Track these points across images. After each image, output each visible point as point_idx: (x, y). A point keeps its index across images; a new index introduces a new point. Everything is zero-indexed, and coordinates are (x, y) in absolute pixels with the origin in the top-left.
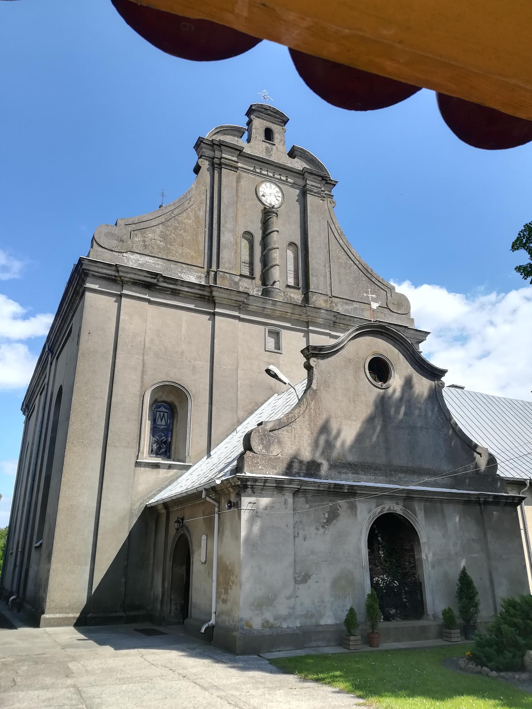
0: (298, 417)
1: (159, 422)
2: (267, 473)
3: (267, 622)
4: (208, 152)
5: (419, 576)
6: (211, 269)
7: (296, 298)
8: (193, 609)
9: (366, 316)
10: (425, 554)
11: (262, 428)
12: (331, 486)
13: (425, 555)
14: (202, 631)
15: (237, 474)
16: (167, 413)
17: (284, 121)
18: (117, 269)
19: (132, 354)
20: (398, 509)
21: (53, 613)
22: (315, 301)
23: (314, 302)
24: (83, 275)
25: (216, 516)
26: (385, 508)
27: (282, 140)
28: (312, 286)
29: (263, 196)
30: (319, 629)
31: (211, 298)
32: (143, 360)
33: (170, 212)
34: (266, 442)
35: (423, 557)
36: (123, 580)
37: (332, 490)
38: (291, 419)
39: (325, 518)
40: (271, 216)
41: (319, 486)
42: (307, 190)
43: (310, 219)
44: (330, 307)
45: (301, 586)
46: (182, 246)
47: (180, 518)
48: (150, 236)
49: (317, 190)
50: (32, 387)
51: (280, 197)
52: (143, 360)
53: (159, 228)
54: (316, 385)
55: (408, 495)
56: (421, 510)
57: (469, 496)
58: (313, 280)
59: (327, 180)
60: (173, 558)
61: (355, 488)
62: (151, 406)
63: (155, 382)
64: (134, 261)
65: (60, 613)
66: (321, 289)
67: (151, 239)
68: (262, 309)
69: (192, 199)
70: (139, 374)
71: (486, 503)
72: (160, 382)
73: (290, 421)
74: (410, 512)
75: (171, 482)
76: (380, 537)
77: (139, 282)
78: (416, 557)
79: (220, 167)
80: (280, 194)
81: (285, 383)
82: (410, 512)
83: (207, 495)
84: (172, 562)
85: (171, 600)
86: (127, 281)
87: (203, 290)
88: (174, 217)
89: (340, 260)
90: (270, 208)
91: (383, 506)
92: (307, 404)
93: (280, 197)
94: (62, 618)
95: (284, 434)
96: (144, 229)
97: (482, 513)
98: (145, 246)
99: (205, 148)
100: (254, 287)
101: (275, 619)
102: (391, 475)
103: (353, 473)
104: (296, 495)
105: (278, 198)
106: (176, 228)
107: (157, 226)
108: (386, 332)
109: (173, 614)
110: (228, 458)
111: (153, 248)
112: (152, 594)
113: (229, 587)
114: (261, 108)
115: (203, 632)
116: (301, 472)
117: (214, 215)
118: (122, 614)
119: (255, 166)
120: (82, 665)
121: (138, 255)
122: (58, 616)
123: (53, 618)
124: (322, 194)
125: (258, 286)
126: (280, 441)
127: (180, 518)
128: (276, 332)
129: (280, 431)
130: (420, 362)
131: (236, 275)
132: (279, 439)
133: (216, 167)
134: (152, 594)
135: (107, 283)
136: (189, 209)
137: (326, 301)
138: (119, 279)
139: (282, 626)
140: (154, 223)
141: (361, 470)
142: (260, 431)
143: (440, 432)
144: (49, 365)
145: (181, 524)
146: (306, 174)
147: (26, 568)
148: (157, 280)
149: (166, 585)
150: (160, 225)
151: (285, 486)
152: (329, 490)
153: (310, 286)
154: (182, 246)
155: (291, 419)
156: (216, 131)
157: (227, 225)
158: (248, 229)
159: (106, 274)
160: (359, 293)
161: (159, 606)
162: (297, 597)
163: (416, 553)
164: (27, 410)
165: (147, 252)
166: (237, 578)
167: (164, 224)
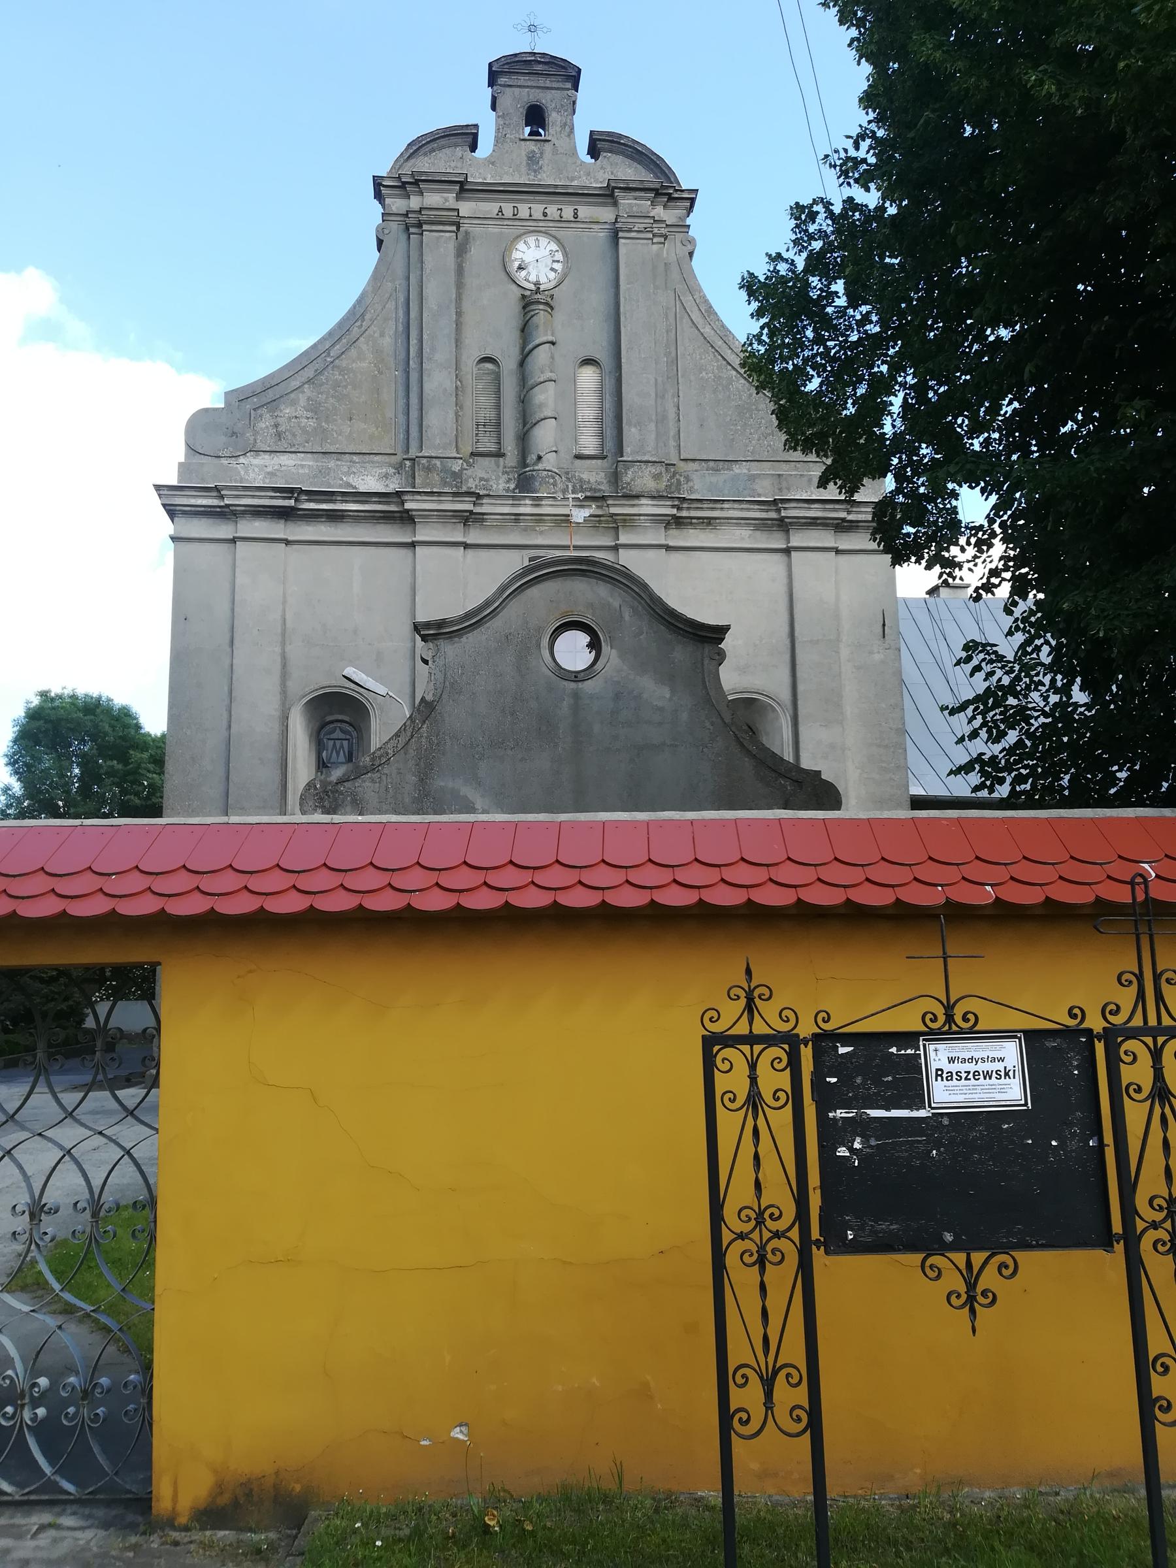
7: (592, 480)
9: (760, 491)
16: (347, 741)
17: (569, 75)
22: (632, 480)
23: (629, 484)
27: (565, 124)
28: (629, 449)
29: (520, 268)
33: (324, 355)
38: (380, 759)
40: (532, 313)
43: (625, 298)
48: (288, 411)
51: (558, 261)
58: (631, 434)
63: (307, 690)
66: (649, 452)
67: (290, 418)
69: (368, 317)
70: (276, 678)
72: (317, 690)
73: (378, 762)
77: (262, 509)
80: (559, 256)
87: (387, 503)
88: (332, 362)
89: (704, 373)
92: (413, 729)
93: (558, 261)
96: (275, 400)
98: (279, 435)
99: (390, 196)
100: (500, 474)
106: (337, 384)
107: (300, 390)
108: (592, 569)
111: (294, 435)
121: (267, 456)
125: (508, 470)
136: (362, 339)
137: (657, 477)
142: (318, 786)
146: (617, 193)
150: (306, 386)
154: (351, 419)
155: (380, 759)
156: (412, 151)
158: (488, 353)
165: (283, 446)
167: (313, 383)
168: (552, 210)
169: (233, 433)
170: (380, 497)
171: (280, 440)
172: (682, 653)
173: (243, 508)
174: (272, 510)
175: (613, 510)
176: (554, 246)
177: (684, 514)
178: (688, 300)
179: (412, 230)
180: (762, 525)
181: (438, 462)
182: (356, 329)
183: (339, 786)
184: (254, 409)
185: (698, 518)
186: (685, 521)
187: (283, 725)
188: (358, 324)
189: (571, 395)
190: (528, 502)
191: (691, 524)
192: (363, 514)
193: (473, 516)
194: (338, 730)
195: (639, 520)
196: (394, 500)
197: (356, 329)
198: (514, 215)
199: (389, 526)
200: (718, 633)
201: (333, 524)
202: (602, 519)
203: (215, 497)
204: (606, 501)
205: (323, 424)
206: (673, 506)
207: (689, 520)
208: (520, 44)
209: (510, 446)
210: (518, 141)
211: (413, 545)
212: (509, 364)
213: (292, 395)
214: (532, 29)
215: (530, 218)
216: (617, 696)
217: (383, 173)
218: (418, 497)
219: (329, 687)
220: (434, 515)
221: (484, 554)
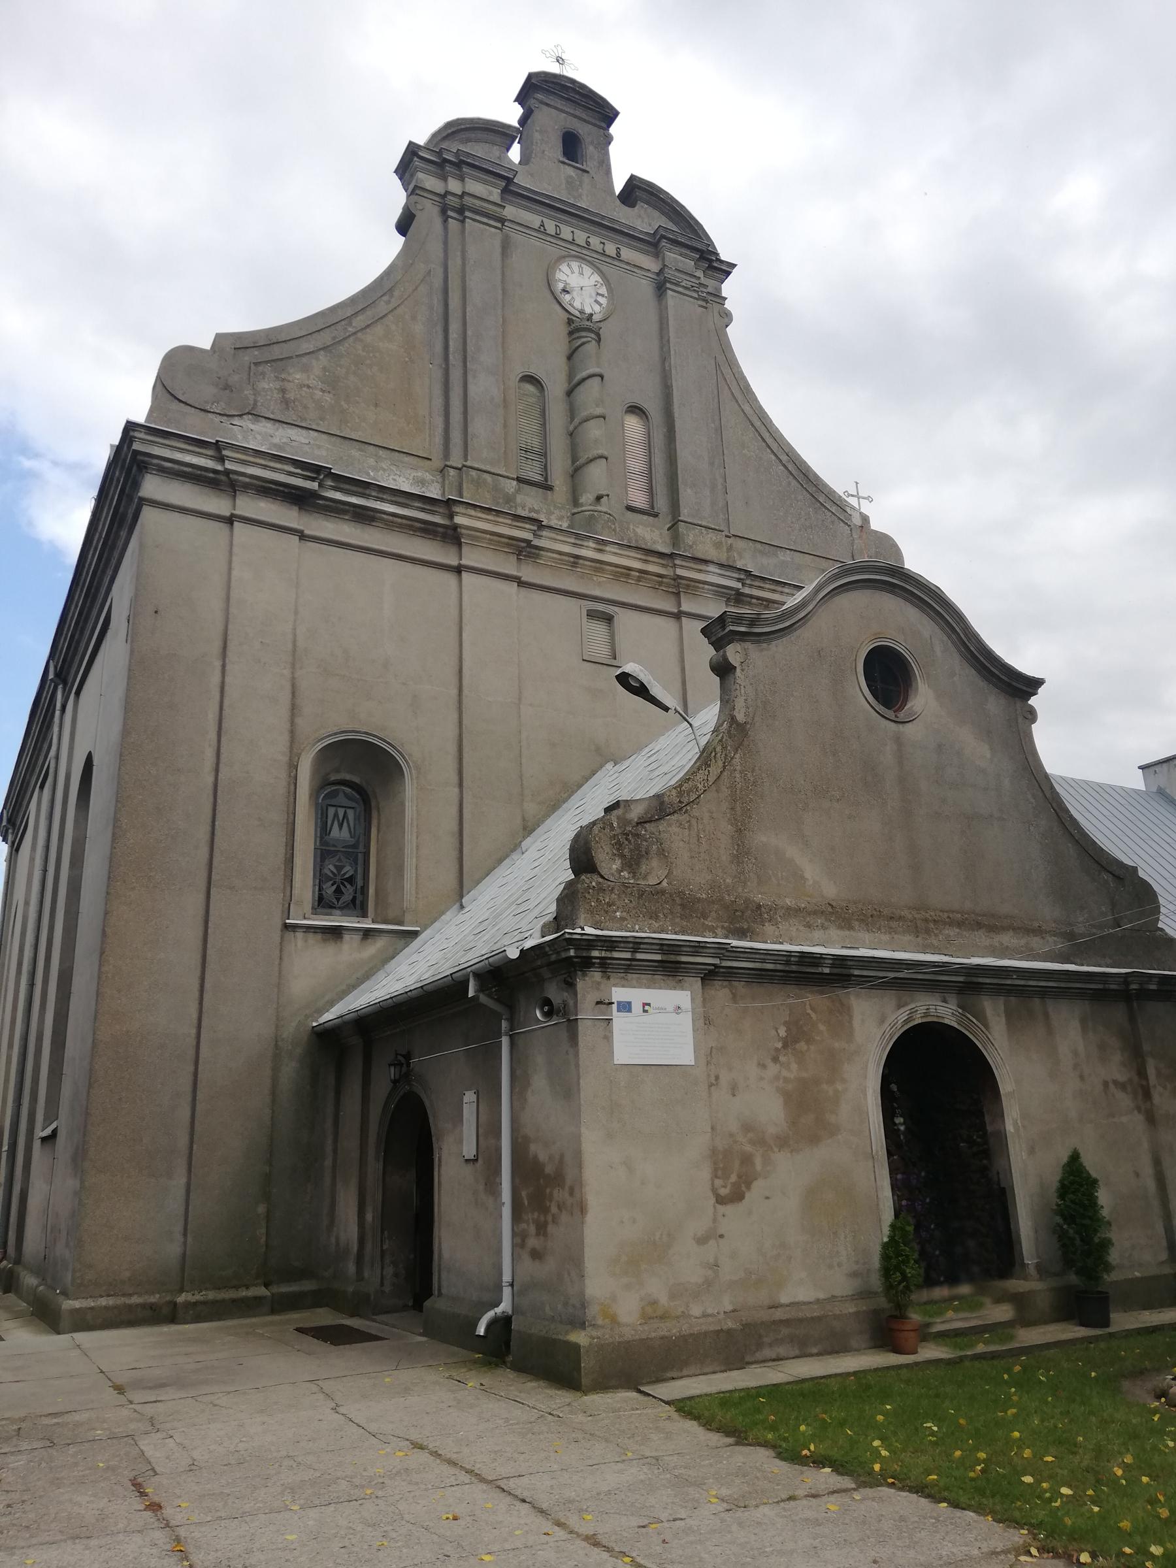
0: (705, 791)
1: (335, 833)
2: (637, 927)
3: (654, 1303)
4: (431, 182)
5: (998, 1173)
6: (448, 463)
8: (444, 1276)
10: (1013, 1120)
11: (618, 818)
12: (792, 959)
13: (1011, 1122)
14: (480, 1331)
15: (567, 931)
19: (265, 663)
20: (946, 1011)
21: (91, 1297)
23: (691, 547)
24: (135, 468)
25: (505, 1041)
26: (917, 1011)
29: (565, 291)
30: (779, 1315)
31: (450, 532)
32: (293, 678)
33: (343, 323)
34: (631, 850)
35: (1007, 1129)
36: (261, 1209)
37: (794, 968)
39: (780, 1039)
41: (763, 961)
42: (666, 280)
44: (728, 559)
45: (728, 1209)
46: (376, 405)
47: (401, 1055)
49: (691, 283)
50: (21, 773)
51: (603, 296)
52: (293, 678)
53: (317, 359)
54: (743, 710)
56: (999, 1015)
57: (1104, 979)
58: (687, 495)
59: (711, 261)
60: (385, 1152)
61: (849, 963)
62: (315, 793)
63: (323, 732)
64: (259, 437)
65: (108, 1296)
67: (301, 386)
69: (396, 293)
70: (284, 711)
71: (1144, 995)
73: (685, 800)
74: (974, 1020)
75: (367, 974)
76: (894, 1083)
77: (274, 487)
78: (989, 1128)
79: (461, 218)
80: (603, 290)
81: (666, 709)
82: (974, 1020)
83: (481, 988)
84: (381, 1163)
85: (383, 1252)
88: (355, 333)
91: (913, 1006)
93: (603, 296)
94: (116, 1307)
95: (672, 831)
97: (1132, 1019)
98: (286, 403)
101: (672, 1297)
102: (928, 931)
103: (840, 928)
104: (707, 982)
105: (600, 299)
109: (387, 1288)
110: (519, 901)
112: (333, 1240)
113: (550, 1218)
114: (553, 83)
115: (482, 1334)
116: (717, 926)
117: (450, 331)
118: (262, 1291)
119: (544, 219)
120: (179, 1444)
121: (269, 425)
122: (103, 1302)
123: (92, 1308)
124: (700, 293)
126: (663, 850)
127: (401, 1055)
128: (605, 617)
129: (662, 825)
130: (982, 659)
131: (508, 477)
132: (661, 844)
133: (452, 218)
134: (333, 1240)
135: (196, 488)
137: (718, 545)
138: (223, 478)
139: (691, 1313)
140: (306, 346)
141: (857, 920)
142: (615, 824)
143: (1032, 828)
144: (57, 713)
145: (404, 1069)
146: (664, 243)
147: (22, 1190)
149: (369, 1217)
151: (684, 959)
152: (787, 969)
153: (681, 509)
158: (533, 370)
160: (790, 529)
161: (351, 1268)
162: (721, 1236)
163: (987, 1119)
164: (10, 831)
165: (291, 417)
166: (571, 1193)
168: (595, 241)
169: (227, 385)
170: (424, 503)
171: (288, 408)
172: (995, 704)
173: (247, 480)
174: (286, 490)
175: (679, 572)
176: (596, 278)
177: (747, 591)
178: (726, 371)
179: (450, 213)
181: (488, 477)
182: (382, 303)
183: (639, 828)
184: (256, 364)
185: (758, 598)
186: (745, 599)
187: (290, 776)
188: (385, 298)
190: (591, 544)
192: (399, 520)
193: (528, 549)
194: (341, 795)
195: (703, 588)
196: (441, 510)
197: (382, 303)
198: (556, 234)
200: (1032, 685)
202: (664, 580)
203: (211, 457)
204: (674, 559)
205: (343, 403)
206: (739, 580)
207: (749, 599)
208: (554, 68)
209: (558, 480)
210: (556, 161)
211: (458, 570)
212: (556, 387)
213: (304, 360)
214: (560, 60)
215: (573, 242)
216: (940, 748)
217: (421, 140)
218: (472, 512)
219: (353, 731)
220: (485, 538)
221: (537, 596)
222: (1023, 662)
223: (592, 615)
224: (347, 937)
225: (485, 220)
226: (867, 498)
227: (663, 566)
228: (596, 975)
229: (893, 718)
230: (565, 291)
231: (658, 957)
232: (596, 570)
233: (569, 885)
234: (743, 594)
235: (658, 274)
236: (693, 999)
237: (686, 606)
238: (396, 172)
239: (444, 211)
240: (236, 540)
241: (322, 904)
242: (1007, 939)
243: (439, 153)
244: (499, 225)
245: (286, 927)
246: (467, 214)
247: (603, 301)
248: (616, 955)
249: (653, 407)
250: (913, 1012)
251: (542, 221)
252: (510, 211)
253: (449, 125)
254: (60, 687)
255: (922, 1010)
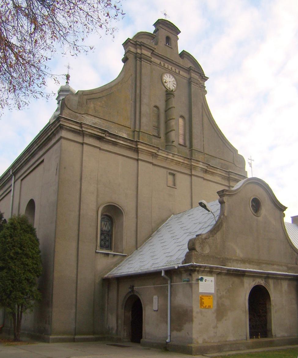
3: (205, 340)
4: (132, 49)
18: (81, 126)
20: (262, 282)
31: (136, 149)
40: (170, 97)
51: (175, 84)
55: (228, 272)
58: (195, 141)
68: (166, 158)
78: (267, 307)
80: (175, 83)
85: (124, 330)
86: (87, 134)
87: (132, 144)
90: (170, 91)
93: (175, 84)
105: (174, 85)
133: (138, 60)
138: (81, 132)
148: (105, 135)
151: (214, 270)
157: (145, 100)
159: (74, 128)
163: (267, 305)
172: (278, 212)
175: (193, 164)
176: (173, 79)
177: (208, 169)
180: (223, 178)
185: (211, 172)
189: (178, 124)
190: (171, 155)
191: (209, 173)
199: (72, 133)
200: (285, 208)
201: (113, 146)
203: (79, 127)
206: (207, 167)
208: (163, 17)
209: (162, 135)
214: (165, 14)
215: (168, 68)
218: (142, 145)
221: (157, 168)
222: (282, 200)
223: (170, 174)
224: (110, 256)
225: (146, 61)
226: (253, 160)
227: (225, 174)
228: (196, 273)
229: (256, 215)
230: (165, 82)
231: (209, 270)
232: (172, 161)
233: (188, 253)
234: (207, 170)
235: (189, 79)
236: (214, 279)
237: (193, 173)
238: (123, 44)
239: (136, 58)
240: (84, 149)
241: (102, 247)
242: (275, 267)
243: (136, 42)
244: (150, 63)
245: (96, 252)
246: (142, 59)
247: (175, 86)
248: (201, 269)
249: (187, 117)
250: (256, 282)
251: (160, 62)
252: (153, 59)
253: (138, 33)
254: (13, 176)
255: (257, 282)
